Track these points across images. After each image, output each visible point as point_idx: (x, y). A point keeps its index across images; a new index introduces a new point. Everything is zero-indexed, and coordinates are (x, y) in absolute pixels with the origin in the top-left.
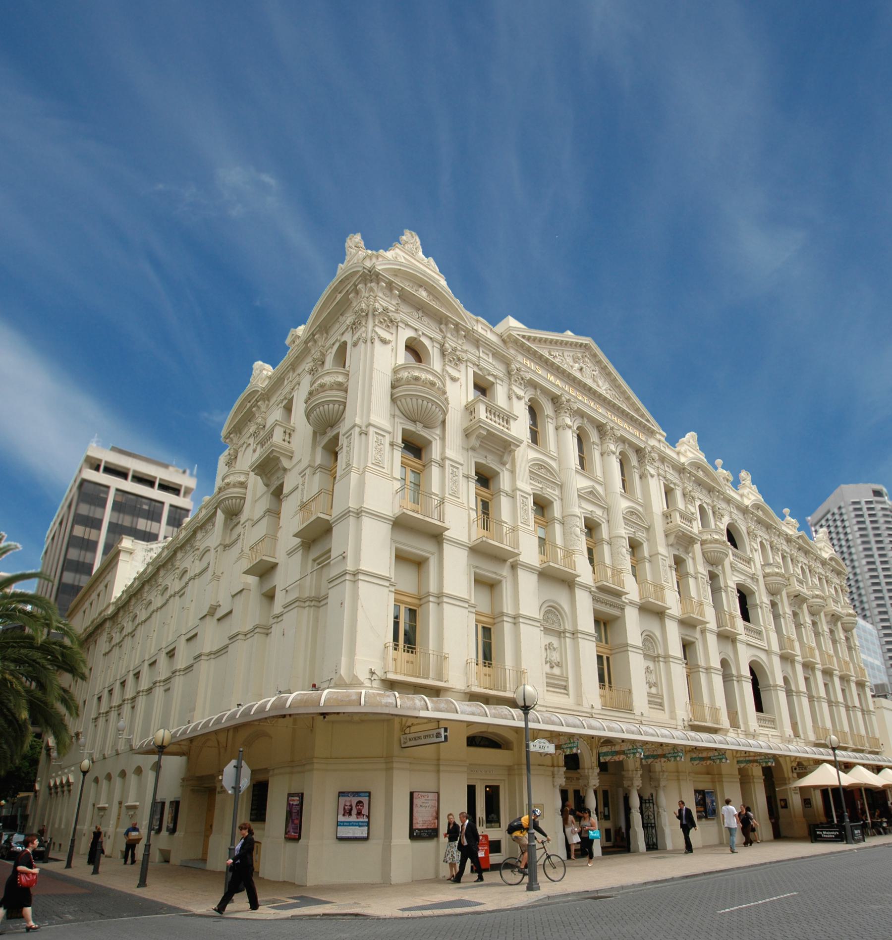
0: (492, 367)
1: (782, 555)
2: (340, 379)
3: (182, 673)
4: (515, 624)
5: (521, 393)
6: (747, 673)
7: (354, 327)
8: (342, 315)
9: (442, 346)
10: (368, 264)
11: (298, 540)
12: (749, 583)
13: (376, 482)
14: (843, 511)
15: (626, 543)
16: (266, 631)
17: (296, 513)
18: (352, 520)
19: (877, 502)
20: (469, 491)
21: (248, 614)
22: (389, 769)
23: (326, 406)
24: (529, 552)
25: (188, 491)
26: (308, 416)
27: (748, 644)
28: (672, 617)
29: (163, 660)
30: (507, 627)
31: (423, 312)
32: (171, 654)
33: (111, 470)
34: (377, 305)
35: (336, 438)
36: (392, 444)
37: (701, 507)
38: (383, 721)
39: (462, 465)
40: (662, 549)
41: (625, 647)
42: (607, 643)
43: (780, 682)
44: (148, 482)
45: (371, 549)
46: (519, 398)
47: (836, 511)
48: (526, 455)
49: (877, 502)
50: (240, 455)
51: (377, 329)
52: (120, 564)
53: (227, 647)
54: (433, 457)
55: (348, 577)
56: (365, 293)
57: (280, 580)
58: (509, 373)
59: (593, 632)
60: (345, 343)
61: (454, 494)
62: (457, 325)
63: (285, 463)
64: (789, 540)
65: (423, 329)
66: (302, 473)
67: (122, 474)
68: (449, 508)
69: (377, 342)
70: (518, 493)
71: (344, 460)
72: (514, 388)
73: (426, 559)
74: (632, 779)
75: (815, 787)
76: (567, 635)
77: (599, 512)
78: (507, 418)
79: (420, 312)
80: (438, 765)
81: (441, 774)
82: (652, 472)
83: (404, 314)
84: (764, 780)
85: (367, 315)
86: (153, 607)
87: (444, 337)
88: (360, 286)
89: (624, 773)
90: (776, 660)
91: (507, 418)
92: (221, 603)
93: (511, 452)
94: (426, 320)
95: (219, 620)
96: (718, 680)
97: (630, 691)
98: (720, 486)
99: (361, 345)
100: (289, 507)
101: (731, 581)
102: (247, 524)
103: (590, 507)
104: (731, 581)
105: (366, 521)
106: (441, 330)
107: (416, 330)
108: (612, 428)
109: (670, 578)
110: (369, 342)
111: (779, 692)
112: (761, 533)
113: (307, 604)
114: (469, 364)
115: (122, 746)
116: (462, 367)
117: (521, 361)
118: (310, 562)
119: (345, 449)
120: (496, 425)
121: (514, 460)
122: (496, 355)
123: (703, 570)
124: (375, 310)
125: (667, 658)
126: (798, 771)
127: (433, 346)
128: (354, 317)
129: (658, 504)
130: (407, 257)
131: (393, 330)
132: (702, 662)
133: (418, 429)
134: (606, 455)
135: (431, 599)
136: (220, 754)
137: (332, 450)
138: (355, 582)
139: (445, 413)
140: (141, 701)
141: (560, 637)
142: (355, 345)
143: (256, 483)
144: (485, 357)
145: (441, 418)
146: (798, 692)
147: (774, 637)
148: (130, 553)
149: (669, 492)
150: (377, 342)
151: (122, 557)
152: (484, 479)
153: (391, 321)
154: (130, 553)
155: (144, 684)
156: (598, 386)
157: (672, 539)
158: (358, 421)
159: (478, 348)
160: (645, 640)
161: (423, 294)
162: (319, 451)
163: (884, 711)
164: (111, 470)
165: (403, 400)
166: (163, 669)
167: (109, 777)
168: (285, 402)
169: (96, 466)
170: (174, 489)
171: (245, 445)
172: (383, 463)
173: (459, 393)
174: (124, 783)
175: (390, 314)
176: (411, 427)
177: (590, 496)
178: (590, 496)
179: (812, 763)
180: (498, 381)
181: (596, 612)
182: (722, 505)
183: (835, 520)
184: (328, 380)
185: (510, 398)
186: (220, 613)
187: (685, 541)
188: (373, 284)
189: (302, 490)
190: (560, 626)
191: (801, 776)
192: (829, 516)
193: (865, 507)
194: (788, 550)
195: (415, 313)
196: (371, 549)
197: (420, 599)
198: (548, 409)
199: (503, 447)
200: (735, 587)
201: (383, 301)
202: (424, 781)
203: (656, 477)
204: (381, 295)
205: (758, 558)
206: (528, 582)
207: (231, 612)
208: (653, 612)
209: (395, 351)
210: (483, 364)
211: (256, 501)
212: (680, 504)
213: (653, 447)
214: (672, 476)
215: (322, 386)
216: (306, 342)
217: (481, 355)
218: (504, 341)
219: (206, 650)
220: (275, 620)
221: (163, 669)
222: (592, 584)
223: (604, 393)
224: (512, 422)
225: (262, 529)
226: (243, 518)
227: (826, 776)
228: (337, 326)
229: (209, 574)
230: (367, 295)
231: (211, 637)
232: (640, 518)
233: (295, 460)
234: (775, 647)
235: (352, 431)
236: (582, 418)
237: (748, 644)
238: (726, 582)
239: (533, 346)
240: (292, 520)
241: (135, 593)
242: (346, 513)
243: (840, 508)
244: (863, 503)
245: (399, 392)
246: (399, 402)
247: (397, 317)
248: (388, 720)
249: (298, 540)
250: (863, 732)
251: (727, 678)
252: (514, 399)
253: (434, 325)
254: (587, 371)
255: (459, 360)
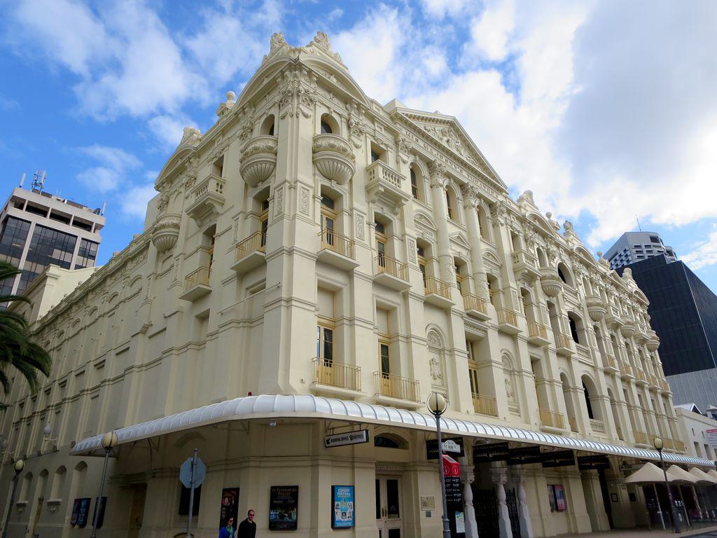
0: (385, 138)
1: (599, 288)
2: (271, 144)
3: (111, 383)
4: (407, 343)
5: (405, 158)
6: (559, 379)
7: (281, 104)
8: (269, 94)
9: (348, 121)
10: (293, 56)
11: (234, 272)
12: (577, 311)
13: (303, 228)
14: (628, 253)
15: (452, 262)
16: (200, 345)
17: (230, 250)
18: (285, 257)
19: (654, 246)
20: (370, 236)
21: (182, 331)
22: (315, 466)
23: (264, 165)
24: (415, 281)
25: (99, 227)
26: (242, 173)
27: (579, 361)
28: (522, 338)
29: (91, 369)
30: (402, 345)
31: (333, 94)
32: (100, 366)
33: (33, 209)
34: (301, 88)
35: (267, 190)
36: (314, 197)
37: (538, 250)
38: (308, 424)
39: (365, 214)
40: (513, 284)
41: (489, 363)
42: (473, 359)
43: (606, 393)
44: (64, 219)
45: (303, 279)
46: (404, 162)
47: (623, 253)
48: (412, 208)
49: (654, 246)
50: (171, 201)
51: (301, 106)
52: (47, 288)
53: (160, 359)
54: (344, 207)
55: (283, 303)
56: (290, 79)
57: (212, 305)
58: (396, 143)
59: (465, 350)
60: (272, 117)
61: (361, 237)
62: (359, 105)
63: (218, 208)
64: (604, 277)
65: (333, 107)
66: (235, 218)
67: (42, 211)
68: (357, 248)
69: (301, 116)
70: (407, 237)
71: (276, 209)
72: (400, 154)
73: (340, 290)
74: (499, 475)
75: (640, 484)
76: (446, 352)
77: (464, 253)
78: (398, 179)
79: (331, 94)
80: (353, 462)
81: (356, 470)
82: (502, 221)
83: (321, 95)
84: (599, 477)
85: (292, 95)
86: (80, 325)
87: (349, 114)
88: (287, 73)
89: (491, 469)
90: (601, 375)
91: (398, 179)
92: (153, 323)
93: (401, 206)
94: (336, 101)
95: (150, 337)
96: (559, 390)
97: (495, 399)
98: (550, 231)
99: (288, 118)
100: (221, 245)
101: (564, 309)
102: (180, 257)
103: (458, 249)
104: (564, 309)
105: (296, 257)
106: (347, 109)
107: (328, 107)
108: (472, 187)
109: (519, 307)
110: (295, 116)
111: (606, 402)
112: (584, 271)
113: (241, 325)
114: (367, 135)
115: (44, 448)
116: (362, 137)
117: (403, 132)
118: (243, 291)
119: (276, 200)
120: (390, 183)
121: (402, 211)
122: (388, 129)
123: (543, 300)
124: (299, 91)
125: (520, 372)
126: (624, 469)
127: (341, 121)
128: (281, 96)
129: (507, 247)
130: (321, 52)
131: (312, 107)
132: (546, 376)
133: (333, 185)
134: (467, 208)
135: (345, 322)
136: (151, 453)
137: (264, 201)
138: (289, 307)
139: (353, 174)
140: (67, 408)
141: (440, 354)
142: (283, 117)
143: (188, 225)
144: (379, 130)
145: (350, 177)
146: (620, 402)
147: (598, 355)
148: (56, 278)
149: (514, 237)
150: (301, 116)
151: (49, 281)
152: (381, 225)
153: (311, 101)
154: (56, 278)
155: (71, 391)
156: (461, 154)
157: (519, 275)
158: (288, 178)
159: (373, 123)
160: (503, 357)
161: (333, 80)
162: (250, 201)
163: (685, 418)
164: (33, 209)
165: (322, 163)
166: (91, 379)
167: (62, 470)
168: (215, 160)
169: (19, 204)
170: (86, 226)
171: (176, 193)
172: (308, 211)
173: (362, 158)
174: (29, 485)
175: (311, 95)
176: (327, 183)
177: (459, 241)
178: (459, 241)
179: (634, 462)
180: (389, 149)
181: (467, 334)
182: (553, 248)
183: (622, 261)
184: (260, 144)
185: (397, 162)
186: (152, 331)
187: (530, 277)
188: (297, 72)
189: (236, 231)
190: (440, 345)
191: (627, 474)
192: (617, 257)
193: (645, 250)
194: (604, 285)
195: (327, 94)
196: (303, 279)
197: (335, 322)
198: (425, 171)
199: (394, 201)
200: (567, 314)
201: (305, 85)
202: (342, 478)
203: (505, 226)
204: (303, 80)
205: (582, 290)
206: (416, 308)
207: (165, 329)
208: (509, 334)
209: (314, 122)
210: (378, 136)
211: (187, 239)
212: (523, 245)
213: (502, 202)
214: (517, 225)
215: (256, 149)
216: (236, 114)
217: (377, 128)
218: (391, 118)
219: (138, 363)
220: (209, 338)
221: (91, 379)
222: (464, 311)
223: (465, 159)
224: (402, 180)
225: (196, 262)
226: (176, 251)
227: (651, 474)
228: (264, 103)
229: (139, 300)
230: (292, 80)
231: (142, 351)
232: (495, 259)
233: (227, 206)
234: (600, 364)
235: (283, 186)
236: (480, 198)
237: (579, 361)
238: (560, 310)
239: (415, 122)
240: (226, 258)
241: (61, 313)
242: (280, 251)
243: (625, 251)
244: (643, 247)
245: (319, 156)
246: (318, 164)
247: (316, 98)
248: (313, 423)
249: (234, 272)
250: (670, 437)
251: (566, 389)
252: (401, 163)
253: (341, 105)
254: (453, 143)
255: (361, 132)
